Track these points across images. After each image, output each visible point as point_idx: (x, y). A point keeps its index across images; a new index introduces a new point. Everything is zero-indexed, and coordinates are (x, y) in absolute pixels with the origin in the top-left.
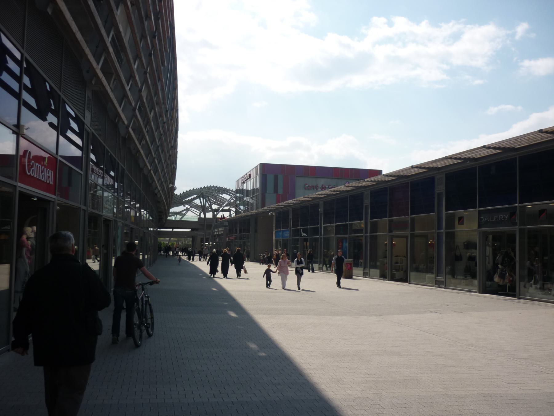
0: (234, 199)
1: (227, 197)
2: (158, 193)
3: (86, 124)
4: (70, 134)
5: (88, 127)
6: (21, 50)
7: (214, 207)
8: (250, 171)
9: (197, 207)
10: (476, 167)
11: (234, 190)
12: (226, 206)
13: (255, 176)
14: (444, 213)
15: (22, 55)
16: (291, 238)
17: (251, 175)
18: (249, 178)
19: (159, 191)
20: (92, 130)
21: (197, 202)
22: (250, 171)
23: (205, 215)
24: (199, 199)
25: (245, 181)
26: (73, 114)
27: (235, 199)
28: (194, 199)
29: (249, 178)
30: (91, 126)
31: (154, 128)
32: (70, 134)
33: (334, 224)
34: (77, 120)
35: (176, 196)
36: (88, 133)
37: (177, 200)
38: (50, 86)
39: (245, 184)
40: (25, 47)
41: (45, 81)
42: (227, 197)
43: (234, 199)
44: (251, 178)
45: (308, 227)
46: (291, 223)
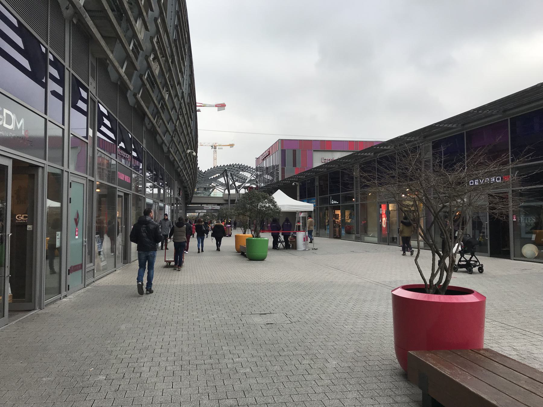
0: (254, 176)
1: (248, 175)
2: (180, 172)
3: (90, 92)
4: (103, 129)
5: (94, 96)
6: (131, 134)
7: (237, 184)
8: (269, 149)
9: (222, 184)
10: (464, 132)
11: (254, 167)
12: (248, 183)
13: (274, 152)
14: (318, 197)
15: (108, 112)
16: (359, 203)
17: (271, 152)
18: (268, 155)
19: (182, 170)
20: (147, 150)
21: (222, 180)
22: (269, 149)
23: (229, 191)
24: (223, 178)
25: (265, 158)
26: (105, 112)
27: (255, 177)
28: (219, 177)
29: (268, 155)
30: (96, 95)
31: (185, 134)
32: (103, 129)
33: (328, 195)
34: (56, 64)
35: (201, 173)
36: (144, 152)
37: (202, 176)
38: (54, 56)
39: (265, 161)
40: (49, 43)
41: (40, 42)
42: (248, 175)
43: (254, 176)
44: (271, 154)
45: (340, 193)
46: (317, 191)
